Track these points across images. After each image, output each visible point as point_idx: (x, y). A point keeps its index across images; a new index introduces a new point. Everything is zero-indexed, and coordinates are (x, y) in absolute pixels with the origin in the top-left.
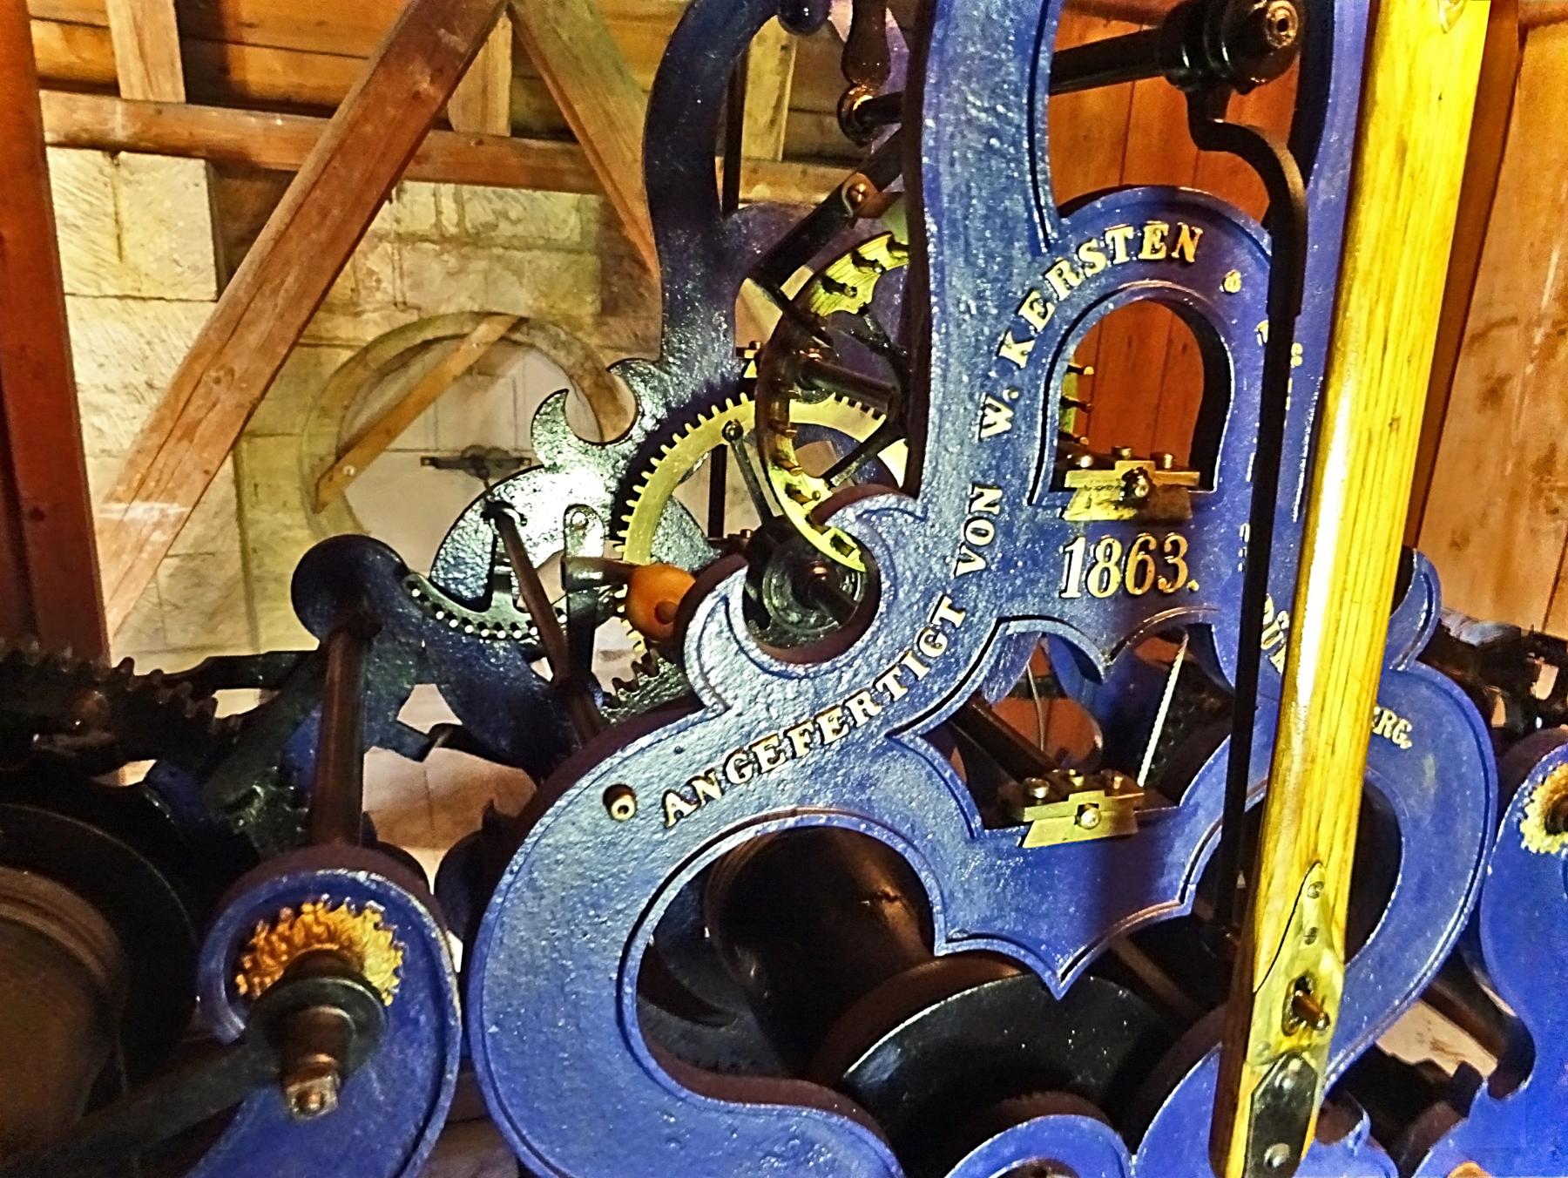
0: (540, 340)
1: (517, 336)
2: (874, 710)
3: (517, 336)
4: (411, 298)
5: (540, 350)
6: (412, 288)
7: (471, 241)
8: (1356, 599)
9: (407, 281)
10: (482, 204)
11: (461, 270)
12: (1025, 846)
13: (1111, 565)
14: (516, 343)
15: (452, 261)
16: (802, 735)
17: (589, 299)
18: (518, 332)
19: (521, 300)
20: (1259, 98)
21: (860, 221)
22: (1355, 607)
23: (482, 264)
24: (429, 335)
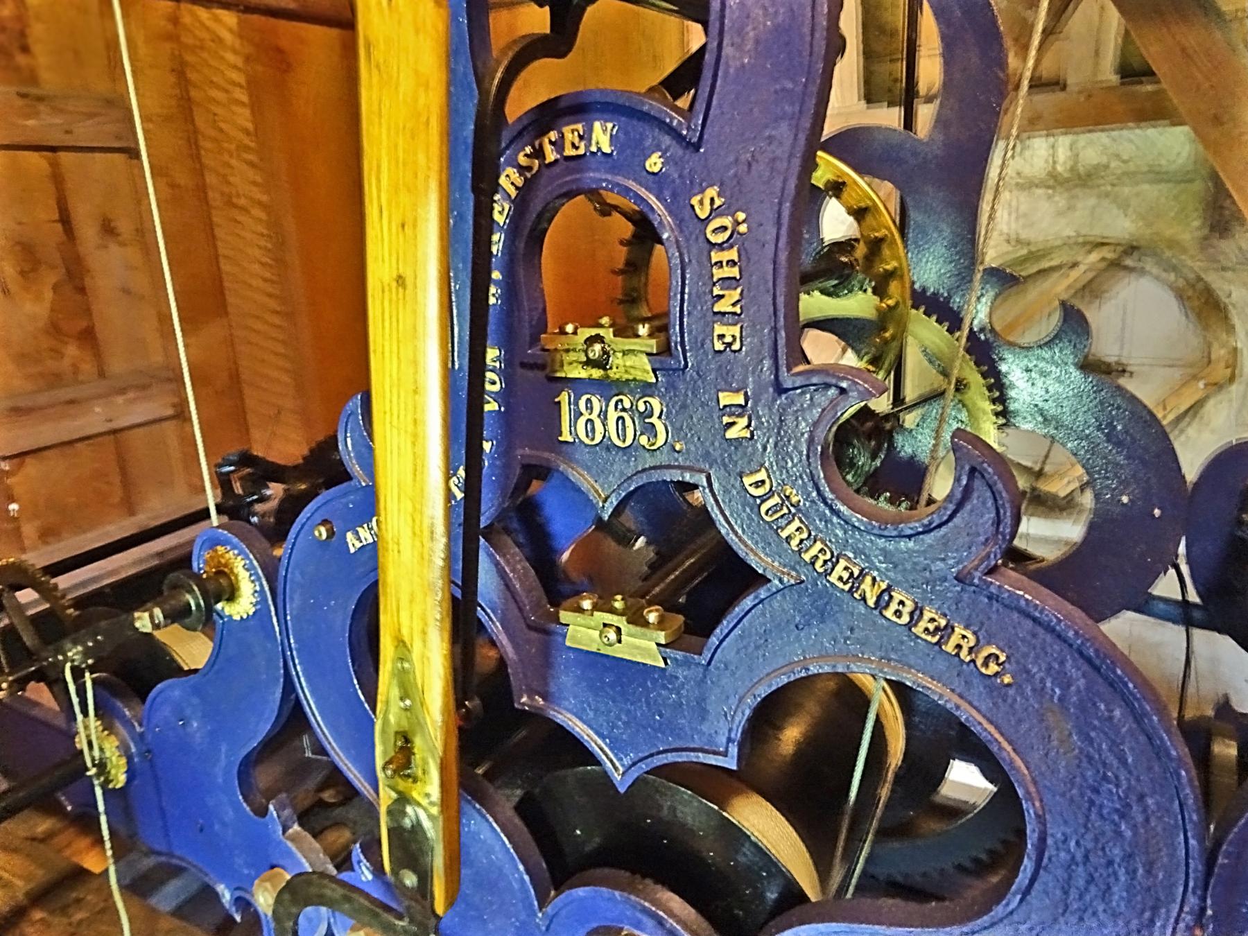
0: (1149, 264)
1: (1129, 262)
2: (794, 543)
3: (1129, 262)
4: (1024, 235)
5: (1150, 273)
6: (1024, 226)
7: (1080, 180)
8: (395, 423)
9: (1022, 221)
10: (1094, 147)
11: (1071, 208)
12: (1172, 571)
13: (594, 416)
14: (1126, 268)
15: (1061, 200)
16: (846, 568)
17: (1196, 223)
18: (1125, 257)
19: (1122, 226)
20: (656, 59)
21: (1024, 160)
22: (395, 431)
23: (1092, 201)
24: (1045, 264)
